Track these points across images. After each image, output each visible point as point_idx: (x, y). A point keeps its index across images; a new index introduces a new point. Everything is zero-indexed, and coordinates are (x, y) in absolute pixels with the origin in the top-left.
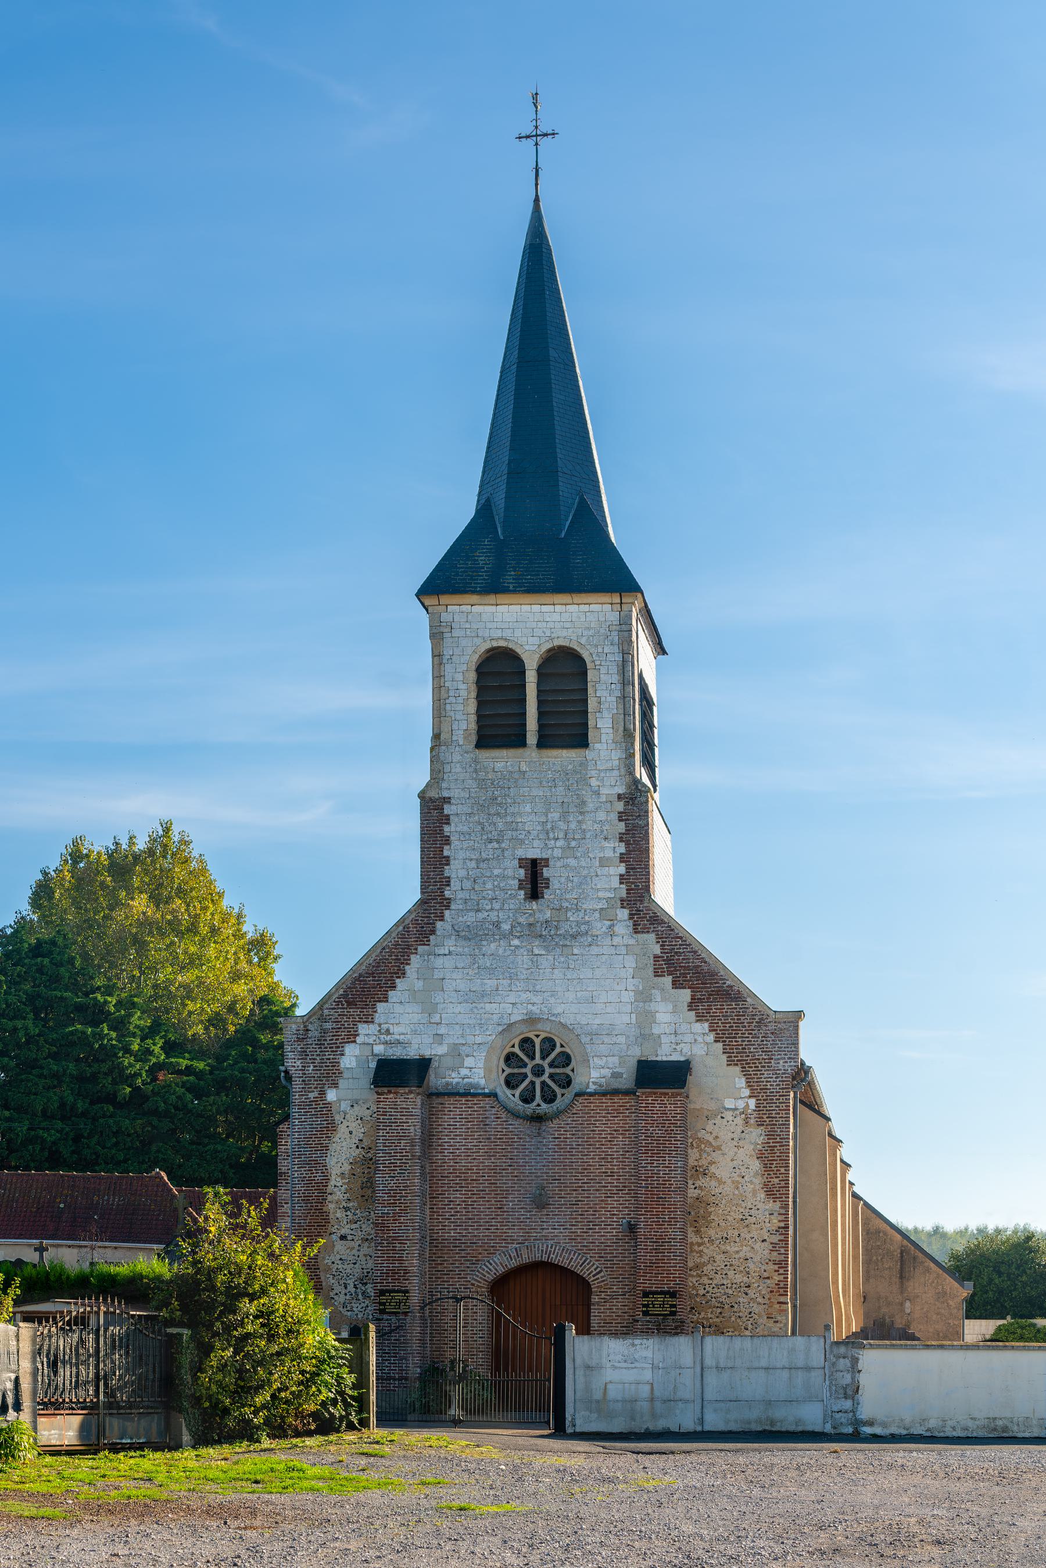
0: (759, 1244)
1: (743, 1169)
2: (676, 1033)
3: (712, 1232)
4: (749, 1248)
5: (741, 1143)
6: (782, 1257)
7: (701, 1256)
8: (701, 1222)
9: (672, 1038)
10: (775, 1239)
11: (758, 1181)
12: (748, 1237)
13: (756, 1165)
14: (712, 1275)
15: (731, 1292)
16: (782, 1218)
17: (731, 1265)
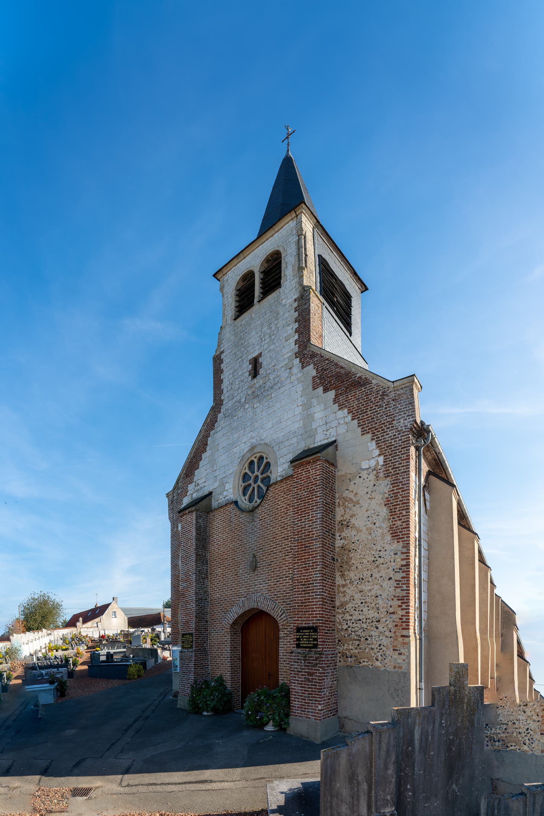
0: (387, 581)
1: (375, 517)
2: (326, 423)
3: (352, 575)
4: (379, 586)
5: (373, 496)
6: (404, 593)
7: (344, 596)
8: (345, 566)
9: (324, 428)
10: (399, 576)
11: (386, 525)
12: (378, 576)
13: (384, 511)
14: (352, 611)
15: (365, 626)
16: (404, 556)
17: (366, 602)
